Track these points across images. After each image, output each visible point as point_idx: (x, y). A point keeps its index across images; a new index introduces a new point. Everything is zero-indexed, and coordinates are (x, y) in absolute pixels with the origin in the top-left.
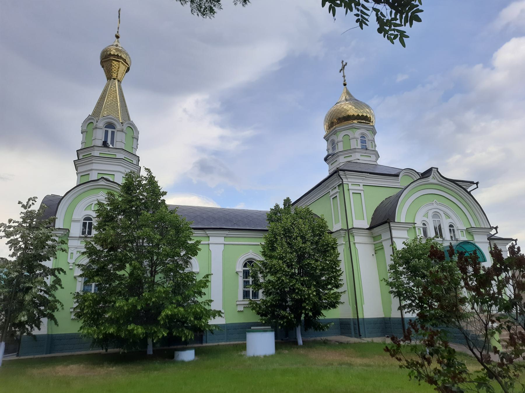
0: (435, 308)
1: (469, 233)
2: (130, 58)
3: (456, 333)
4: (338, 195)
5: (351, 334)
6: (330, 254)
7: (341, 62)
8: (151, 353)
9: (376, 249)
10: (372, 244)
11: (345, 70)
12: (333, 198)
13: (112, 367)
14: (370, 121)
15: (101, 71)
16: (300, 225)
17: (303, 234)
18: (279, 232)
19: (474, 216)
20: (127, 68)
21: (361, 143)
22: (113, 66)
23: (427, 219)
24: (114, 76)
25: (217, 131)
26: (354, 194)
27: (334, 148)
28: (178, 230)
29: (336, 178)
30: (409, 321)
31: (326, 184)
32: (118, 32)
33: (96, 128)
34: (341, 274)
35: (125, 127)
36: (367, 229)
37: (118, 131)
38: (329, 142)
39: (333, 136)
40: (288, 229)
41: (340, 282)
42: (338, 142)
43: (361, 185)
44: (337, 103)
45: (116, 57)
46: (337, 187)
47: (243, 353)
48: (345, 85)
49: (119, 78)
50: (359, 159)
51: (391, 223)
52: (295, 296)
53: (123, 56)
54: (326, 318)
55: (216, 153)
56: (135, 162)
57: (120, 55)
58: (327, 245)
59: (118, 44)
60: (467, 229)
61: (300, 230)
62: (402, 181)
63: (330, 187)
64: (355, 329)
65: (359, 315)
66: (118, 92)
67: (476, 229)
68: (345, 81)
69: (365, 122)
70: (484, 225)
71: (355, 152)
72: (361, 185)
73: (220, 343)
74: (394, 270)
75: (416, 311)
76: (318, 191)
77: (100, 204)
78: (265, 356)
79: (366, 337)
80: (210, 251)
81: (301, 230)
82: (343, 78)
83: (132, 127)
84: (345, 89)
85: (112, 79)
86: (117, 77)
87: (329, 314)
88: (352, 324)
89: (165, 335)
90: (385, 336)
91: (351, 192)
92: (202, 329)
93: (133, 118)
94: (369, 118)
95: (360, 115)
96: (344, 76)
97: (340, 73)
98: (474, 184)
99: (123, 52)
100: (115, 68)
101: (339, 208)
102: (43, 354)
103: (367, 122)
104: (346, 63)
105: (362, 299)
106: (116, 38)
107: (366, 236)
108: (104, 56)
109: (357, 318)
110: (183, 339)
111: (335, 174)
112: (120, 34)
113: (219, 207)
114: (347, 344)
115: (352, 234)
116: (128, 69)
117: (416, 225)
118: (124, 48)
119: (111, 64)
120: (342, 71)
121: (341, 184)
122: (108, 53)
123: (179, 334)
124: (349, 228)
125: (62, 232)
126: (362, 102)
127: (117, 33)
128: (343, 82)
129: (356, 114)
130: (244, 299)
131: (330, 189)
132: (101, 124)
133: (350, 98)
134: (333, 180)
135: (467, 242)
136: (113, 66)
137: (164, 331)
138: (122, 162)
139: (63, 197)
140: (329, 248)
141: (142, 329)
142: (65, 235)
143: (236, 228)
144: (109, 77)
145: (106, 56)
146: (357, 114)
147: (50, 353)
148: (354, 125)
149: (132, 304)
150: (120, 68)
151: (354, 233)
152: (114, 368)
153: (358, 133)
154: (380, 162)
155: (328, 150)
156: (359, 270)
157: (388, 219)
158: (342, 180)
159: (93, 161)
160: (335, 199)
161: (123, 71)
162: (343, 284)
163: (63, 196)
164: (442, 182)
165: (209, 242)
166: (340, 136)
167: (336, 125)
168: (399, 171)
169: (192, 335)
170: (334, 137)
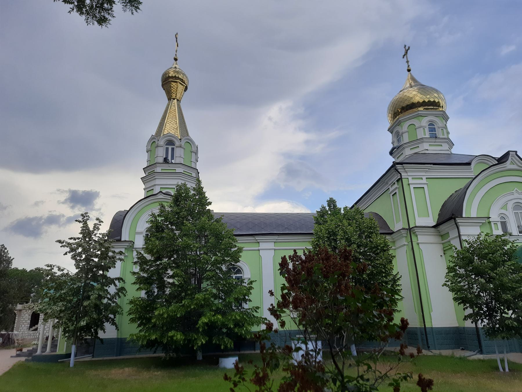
0: (299, 334)
2: (187, 77)
4: (397, 191)
6: (380, 257)
7: (404, 46)
8: (201, 358)
9: (445, 249)
10: (441, 243)
12: (393, 195)
13: (158, 371)
14: (439, 106)
15: (163, 93)
16: (344, 226)
17: (349, 236)
20: (185, 87)
22: (172, 87)
24: (174, 96)
25: (302, 137)
27: (399, 141)
28: (218, 236)
29: (394, 173)
31: (385, 180)
32: (176, 55)
33: (157, 146)
34: (399, 278)
35: (183, 143)
36: (434, 227)
37: (177, 147)
39: (397, 127)
40: (333, 231)
41: (398, 288)
42: (402, 133)
43: (424, 178)
44: (400, 92)
45: (174, 78)
48: (409, 70)
49: (178, 97)
50: (427, 150)
51: (457, 219)
53: (180, 77)
55: (303, 158)
56: (194, 175)
57: (177, 76)
58: (376, 247)
59: (176, 66)
61: (345, 232)
62: (475, 169)
63: (389, 183)
64: (422, 340)
66: (177, 111)
68: (409, 66)
69: (432, 107)
71: (423, 142)
72: (424, 178)
74: (454, 273)
75: (485, 320)
77: (153, 215)
79: (436, 349)
81: (346, 232)
83: (190, 142)
84: (410, 75)
85: (172, 99)
86: (176, 97)
88: (419, 334)
89: (204, 342)
90: (459, 348)
91: (412, 187)
92: (243, 337)
93: (193, 133)
95: (437, 102)
96: (408, 62)
97: (403, 59)
99: (180, 73)
100: (174, 88)
102: (113, 356)
103: (435, 108)
104: (409, 48)
105: (430, 306)
106: (174, 61)
108: (164, 79)
110: (222, 347)
111: (392, 168)
112: (178, 57)
113: (309, 212)
116: (186, 89)
117: (491, 220)
118: (181, 69)
119: (170, 86)
120: (405, 57)
121: (399, 179)
122: (167, 76)
123: (219, 342)
124: (411, 227)
125: (128, 244)
126: (428, 87)
127: (175, 56)
129: (421, 101)
131: (390, 185)
132: (162, 142)
136: (172, 87)
137: (203, 338)
138: (155, 175)
139: (128, 211)
140: (378, 251)
141: (181, 335)
142: (131, 246)
143: (299, 232)
144: (170, 99)
145: (165, 79)
146: (423, 100)
147: (120, 355)
148: (420, 113)
149: (172, 311)
150: (178, 88)
151: (417, 233)
152: (159, 373)
153: (425, 122)
154: (454, 151)
155: (393, 143)
156: (424, 274)
157: (453, 215)
158: (400, 174)
159: (156, 177)
160: (395, 196)
161: (181, 91)
162: (401, 289)
163: (128, 210)
165: (259, 248)
166: (405, 127)
167: (399, 116)
168: (471, 158)
169: (232, 344)
170: (398, 128)
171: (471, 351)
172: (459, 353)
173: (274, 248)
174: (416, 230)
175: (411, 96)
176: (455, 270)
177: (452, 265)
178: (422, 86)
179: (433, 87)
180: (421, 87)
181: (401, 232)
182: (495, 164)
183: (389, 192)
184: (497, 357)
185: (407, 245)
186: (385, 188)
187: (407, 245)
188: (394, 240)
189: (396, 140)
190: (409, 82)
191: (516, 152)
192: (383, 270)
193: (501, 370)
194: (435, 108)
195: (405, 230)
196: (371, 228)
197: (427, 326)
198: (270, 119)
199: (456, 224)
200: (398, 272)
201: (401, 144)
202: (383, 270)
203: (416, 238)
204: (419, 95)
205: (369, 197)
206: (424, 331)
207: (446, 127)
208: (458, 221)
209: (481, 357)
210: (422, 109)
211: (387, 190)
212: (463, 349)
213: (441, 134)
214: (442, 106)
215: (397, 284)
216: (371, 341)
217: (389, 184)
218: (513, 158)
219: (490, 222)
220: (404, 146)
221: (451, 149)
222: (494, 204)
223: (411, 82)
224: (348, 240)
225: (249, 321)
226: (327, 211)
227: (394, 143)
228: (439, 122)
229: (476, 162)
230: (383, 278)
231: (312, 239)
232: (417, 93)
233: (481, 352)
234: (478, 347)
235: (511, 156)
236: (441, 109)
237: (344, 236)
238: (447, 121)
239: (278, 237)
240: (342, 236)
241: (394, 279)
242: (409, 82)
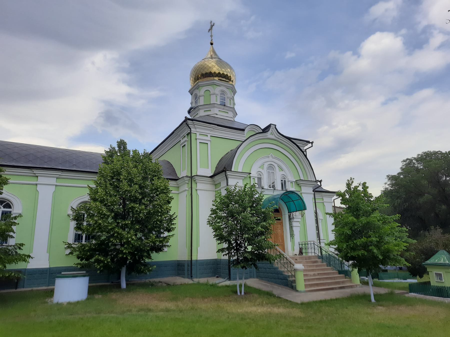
1: (298, 184)
3: (272, 274)
4: (186, 143)
5: (184, 275)
7: (210, 22)
9: (216, 196)
11: (213, 31)
12: (183, 147)
14: (230, 80)
18: (106, 174)
19: (303, 170)
21: (220, 99)
23: (262, 170)
25: (124, 89)
30: (389, 234)
34: (175, 218)
36: (211, 177)
38: (193, 96)
39: (196, 90)
41: (173, 226)
42: (200, 96)
43: (209, 135)
46: (186, 136)
47: (48, 300)
48: (212, 44)
50: (217, 114)
51: (227, 172)
52: (113, 240)
54: (153, 261)
60: (297, 181)
61: (129, 173)
62: (247, 133)
63: (181, 136)
64: (188, 270)
65: (193, 257)
67: (309, 182)
69: (225, 80)
70: (311, 179)
71: (214, 107)
72: (209, 135)
73: (35, 288)
76: (172, 139)
78: (69, 303)
80: (37, 192)
82: (211, 37)
84: (212, 48)
87: (156, 257)
90: (215, 276)
91: (198, 141)
94: (230, 78)
95: (221, 73)
96: (211, 36)
98: (310, 143)
101: (186, 157)
103: (227, 80)
107: (211, 184)
109: (190, 260)
111: (184, 123)
114: (173, 285)
115: (195, 181)
120: (210, 31)
121: (189, 133)
124: (193, 175)
126: (224, 61)
129: (217, 72)
131: (181, 138)
133: (214, 55)
135: (292, 192)
143: (88, 170)
146: (218, 72)
148: (215, 81)
153: (218, 90)
154: (237, 119)
155: (191, 103)
157: (224, 168)
158: (190, 129)
160: (184, 147)
162: (175, 228)
164: (278, 138)
165: (37, 182)
166: (202, 91)
167: (199, 80)
170: (196, 92)
171: (223, 278)
172: (213, 280)
173: (56, 183)
174: (196, 178)
175: (210, 65)
176: (216, 213)
177: (214, 208)
178: (220, 60)
180: (219, 60)
181: (184, 179)
182: (260, 132)
183: (180, 144)
184: (237, 282)
185: (188, 190)
187: (188, 190)
188: (179, 185)
189: (194, 102)
190: (210, 53)
191: (275, 125)
192: (160, 210)
193: (239, 293)
194: (227, 80)
195: (188, 177)
196: (155, 172)
197: (193, 259)
198: (93, 63)
199: (226, 176)
200: (175, 213)
201: (197, 106)
202: (160, 210)
203: (195, 185)
204: (216, 66)
205: (165, 146)
206: (190, 264)
207: (233, 99)
208: (228, 174)
209: (228, 283)
210: (217, 79)
211: (179, 141)
212: (217, 277)
213: (229, 104)
214: (233, 81)
215: (173, 223)
216: (140, 274)
217: (181, 137)
218: (273, 130)
219: (251, 177)
220: (199, 108)
221: (235, 117)
222: (256, 162)
223: (212, 54)
224: (131, 181)
225: (5, 259)
226: (116, 152)
227: (193, 104)
228: (229, 93)
229: (250, 129)
230: (158, 217)
231: (96, 177)
232: (215, 64)
233: (230, 279)
234: (228, 275)
235: (272, 128)
236: (231, 83)
237: (128, 177)
238: (235, 94)
239: (61, 173)
240: (125, 176)
241: (171, 218)
242: (210, 53)
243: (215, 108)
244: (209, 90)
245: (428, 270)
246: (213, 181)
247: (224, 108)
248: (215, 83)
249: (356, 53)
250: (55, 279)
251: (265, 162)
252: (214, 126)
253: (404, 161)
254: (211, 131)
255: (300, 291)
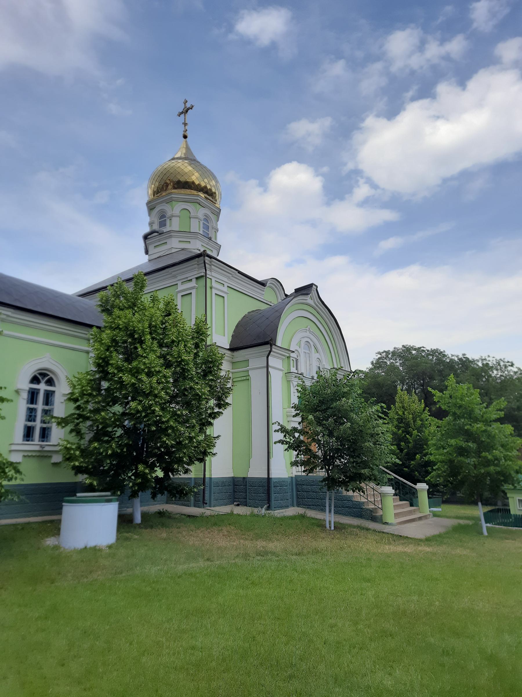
4: (193, 292)
12: (182, 296)
26: (216, 296)
27: (163, 224)
29: (196, 266)
39: (164, 204)
48: (185, 137)
63: (179, 278)
69: (211, 199)
91: (214, 291)
111: (197, 259)
120: (182, 116)
121: (202, 276)
128: (183, 133)
130: (24, 440)
133: (190, 158)
134: (189, 266)
155: (151, 224)
158: (206, 270)
160: (187, 298)
166: (177, 208)
179: (214, 173)
186: (167, 282)
220: (172, 234)
227: (154, 225)
239: (12, 313)
243: (197, 240)
244: (189, 211)
245: (508, 495)
246: (231, 356)
247: (209, 243)
248: (198, 200)
249: (264, 186)
250: (62, 506)
251: (303, 338)
252: (235, 271)
253: (380, 353)
254: (229, 278)
255: (390, 523)
